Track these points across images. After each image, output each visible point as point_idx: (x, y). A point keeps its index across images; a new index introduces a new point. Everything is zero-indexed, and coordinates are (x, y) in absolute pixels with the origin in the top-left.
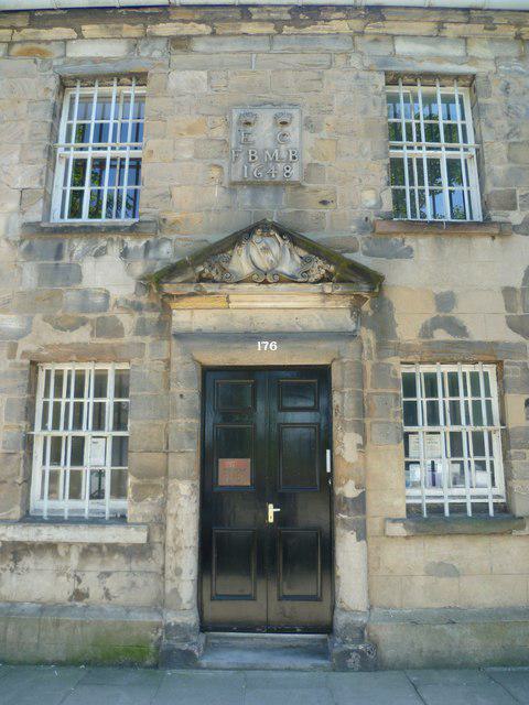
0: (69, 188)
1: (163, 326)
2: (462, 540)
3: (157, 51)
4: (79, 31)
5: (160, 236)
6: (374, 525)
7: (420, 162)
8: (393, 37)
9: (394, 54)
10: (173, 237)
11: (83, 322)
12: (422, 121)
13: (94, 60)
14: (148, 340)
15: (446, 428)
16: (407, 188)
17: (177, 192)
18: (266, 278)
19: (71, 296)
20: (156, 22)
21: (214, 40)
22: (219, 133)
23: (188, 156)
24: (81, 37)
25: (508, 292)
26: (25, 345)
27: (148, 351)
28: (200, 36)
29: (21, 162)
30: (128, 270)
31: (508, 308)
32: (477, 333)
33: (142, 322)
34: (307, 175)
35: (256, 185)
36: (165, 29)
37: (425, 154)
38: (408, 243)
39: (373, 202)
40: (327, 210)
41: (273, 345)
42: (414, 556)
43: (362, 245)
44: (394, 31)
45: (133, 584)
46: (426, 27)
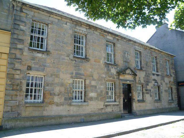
1: (119, 78)
7: (36, 37)
11: (111, 77)
12: (38, 29)
13: (110, 39)
16: (37, 42)
18: (128, 74)
19: (110, 73)
20: (117, 36)
30: (115, 71)
36: (117, 37)
37: (37, 36)
40: (131, 66)
41: (129, 82)
45: (117, 109)
46: (138, 45)
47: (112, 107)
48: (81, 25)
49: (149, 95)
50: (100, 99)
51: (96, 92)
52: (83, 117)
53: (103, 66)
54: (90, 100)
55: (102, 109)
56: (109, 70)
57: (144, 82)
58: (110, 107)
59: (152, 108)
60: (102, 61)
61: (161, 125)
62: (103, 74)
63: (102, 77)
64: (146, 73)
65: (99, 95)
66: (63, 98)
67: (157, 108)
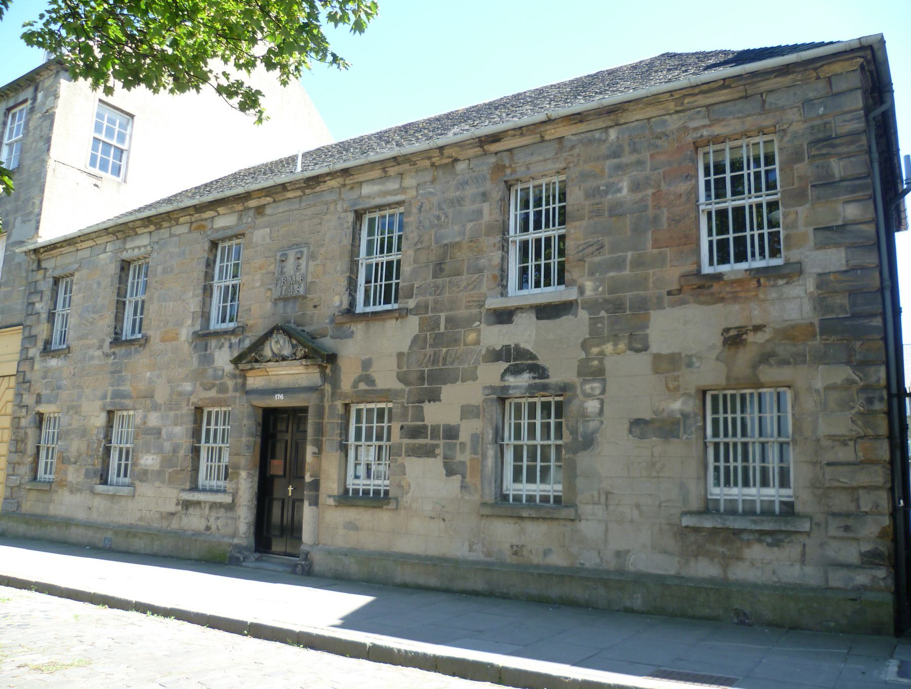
0: (221, 305)
2: (361, 510)
3: (248, 219)
4: (217, 212)
5: (246, 334)
6: (323, 498)
8: (361, 183)
9: (360, 197)
10: (250, 334)
14: (238, 394)
15: (374, 442)
17: (253, 308)
20: (247, 201)
21: (274, 205)
22: (272, 268)
23: (258, 284)
24: (219, 214)
25: (400, 355)
26: (193, 399)
27: (238, 401)
28: (269, 204)
29: (193, 297)
31: (399, 366)
32: (381, 384)
33: (236, 384)
34: (308, 290)
35: (285, 299)
36: (253, 203)
38: (352, 328)
39: (338, 303)
40: (316, 311)
41: (281, 397)
42: (338, 517)
43: (330, 333)
44: (361, 179)
46: (377, 173)
47: (207, 511)
48: (134, 229)
49: (435, 465)
50: (167, 475)
51: (160, 450)
52: (109, 534)
53: (186, 348)
54: (141, 481)
55: (172, 514)
56: (207, 359)
57: (399, 386)
58: (198, 509)
59: (457, 548)
60: (185, 333)
61: (142, 608)
62: (185, 380)
63: (180, 394)
64: (429, 325)
65: (167, 462)
66: (83, 471)
67: (509, 559)
